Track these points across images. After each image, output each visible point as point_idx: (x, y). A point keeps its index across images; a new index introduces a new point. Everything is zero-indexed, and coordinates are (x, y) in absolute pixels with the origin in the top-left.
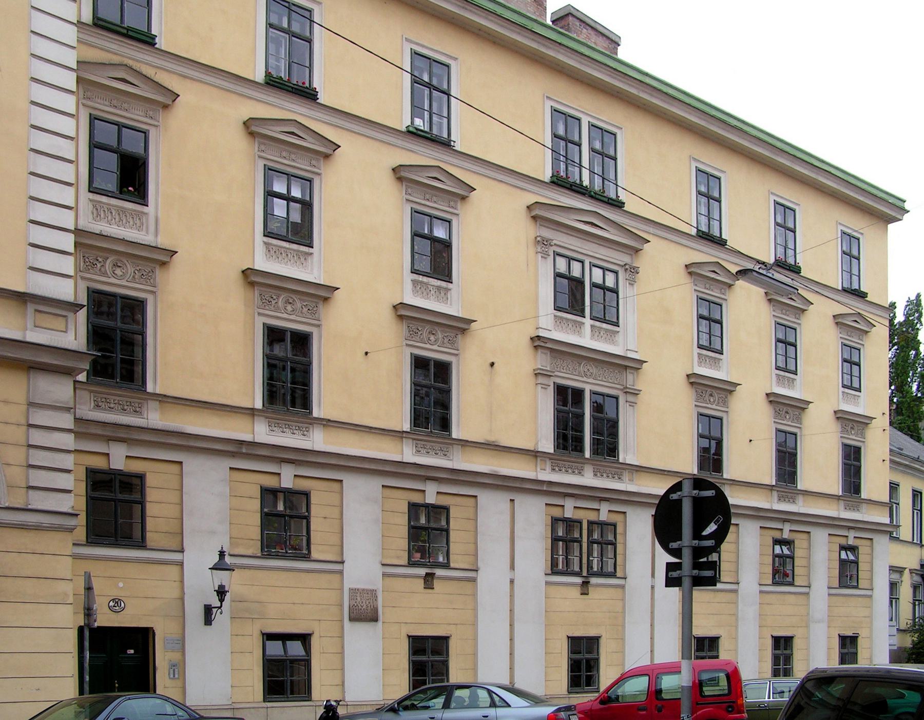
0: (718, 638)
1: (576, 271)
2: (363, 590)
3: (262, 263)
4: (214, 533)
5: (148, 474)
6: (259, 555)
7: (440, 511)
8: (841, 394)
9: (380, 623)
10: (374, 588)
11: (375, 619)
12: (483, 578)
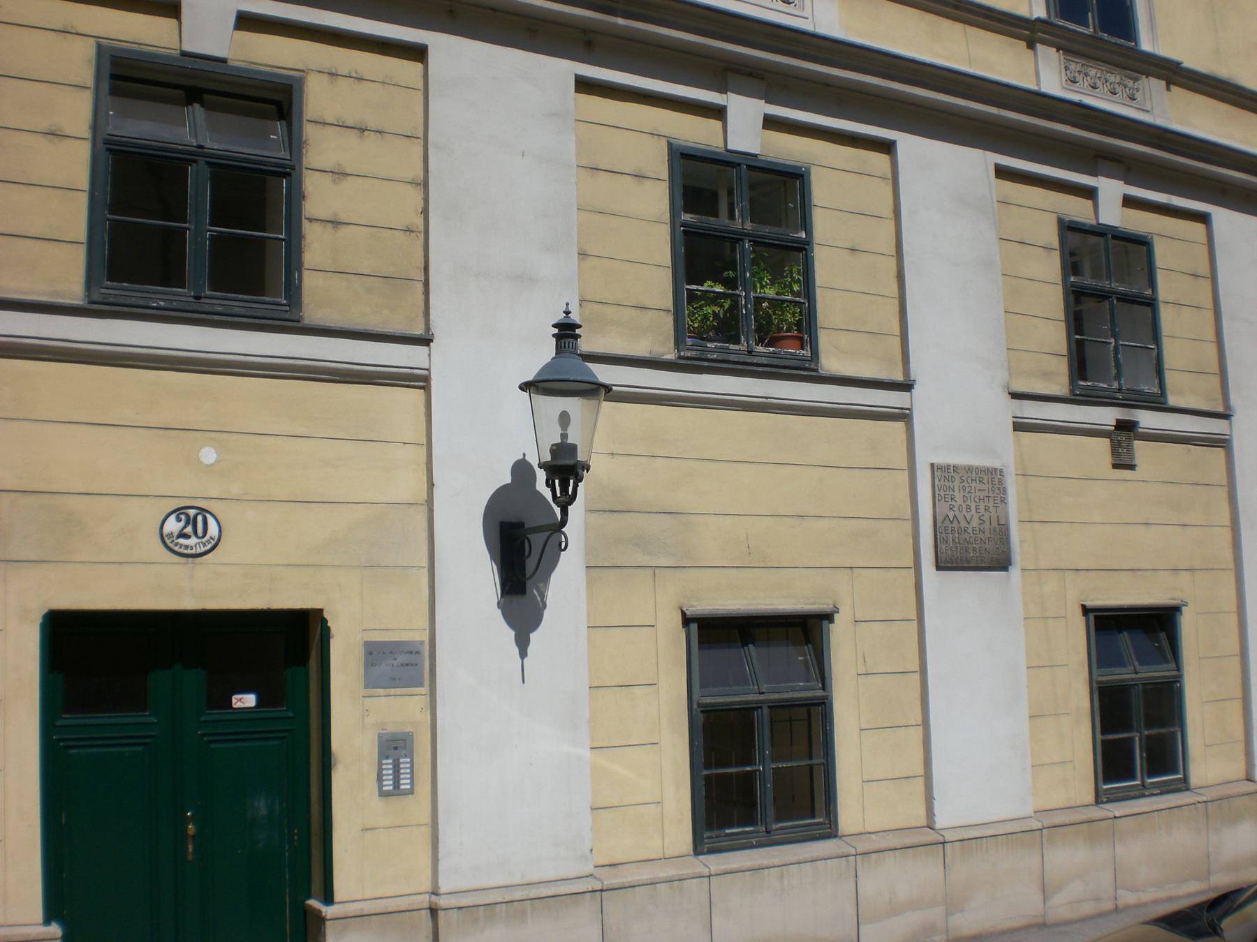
0: (828, 617)
2: (969, 469)
4: (525, 279)
5: (813, 170)
6: (671, 356)
7: (783, 188)
9: (1015, 572)
10: (997, 465)
11: (1002, 563)
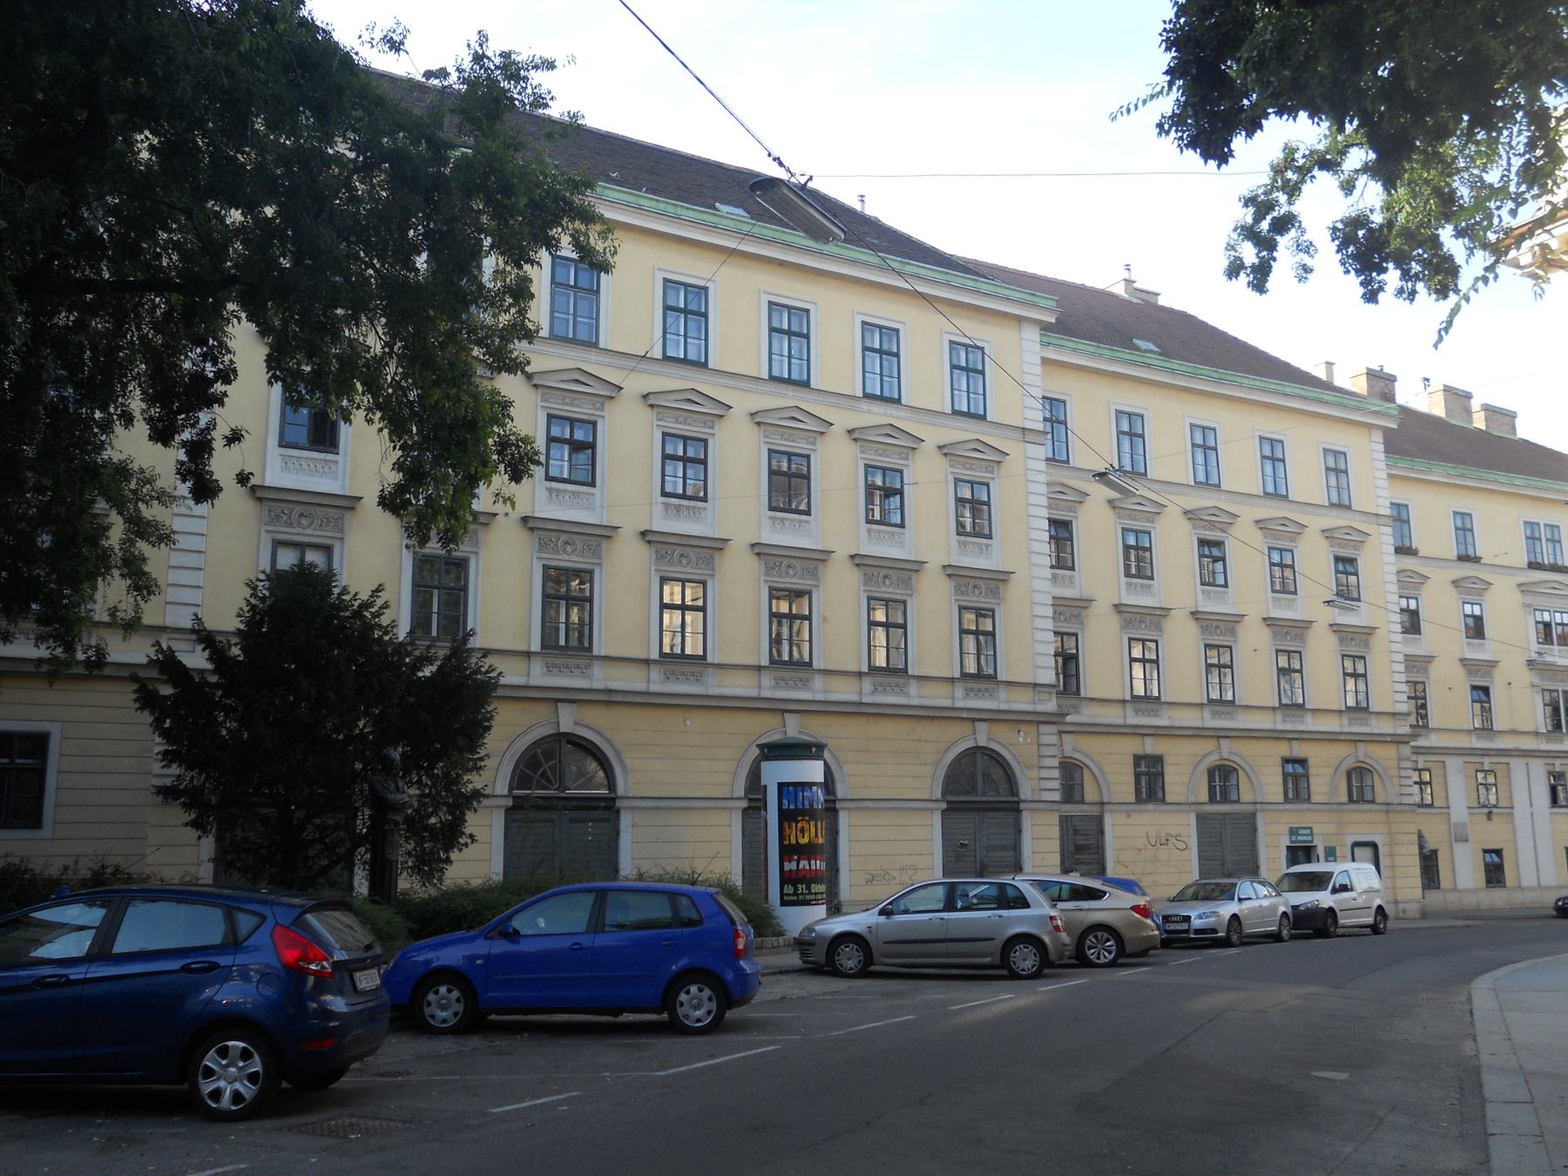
1: (1547, 617)
3: (664, 524)
7: (1157, 760)
8: (1123, 587)
12: (1516, 811)
